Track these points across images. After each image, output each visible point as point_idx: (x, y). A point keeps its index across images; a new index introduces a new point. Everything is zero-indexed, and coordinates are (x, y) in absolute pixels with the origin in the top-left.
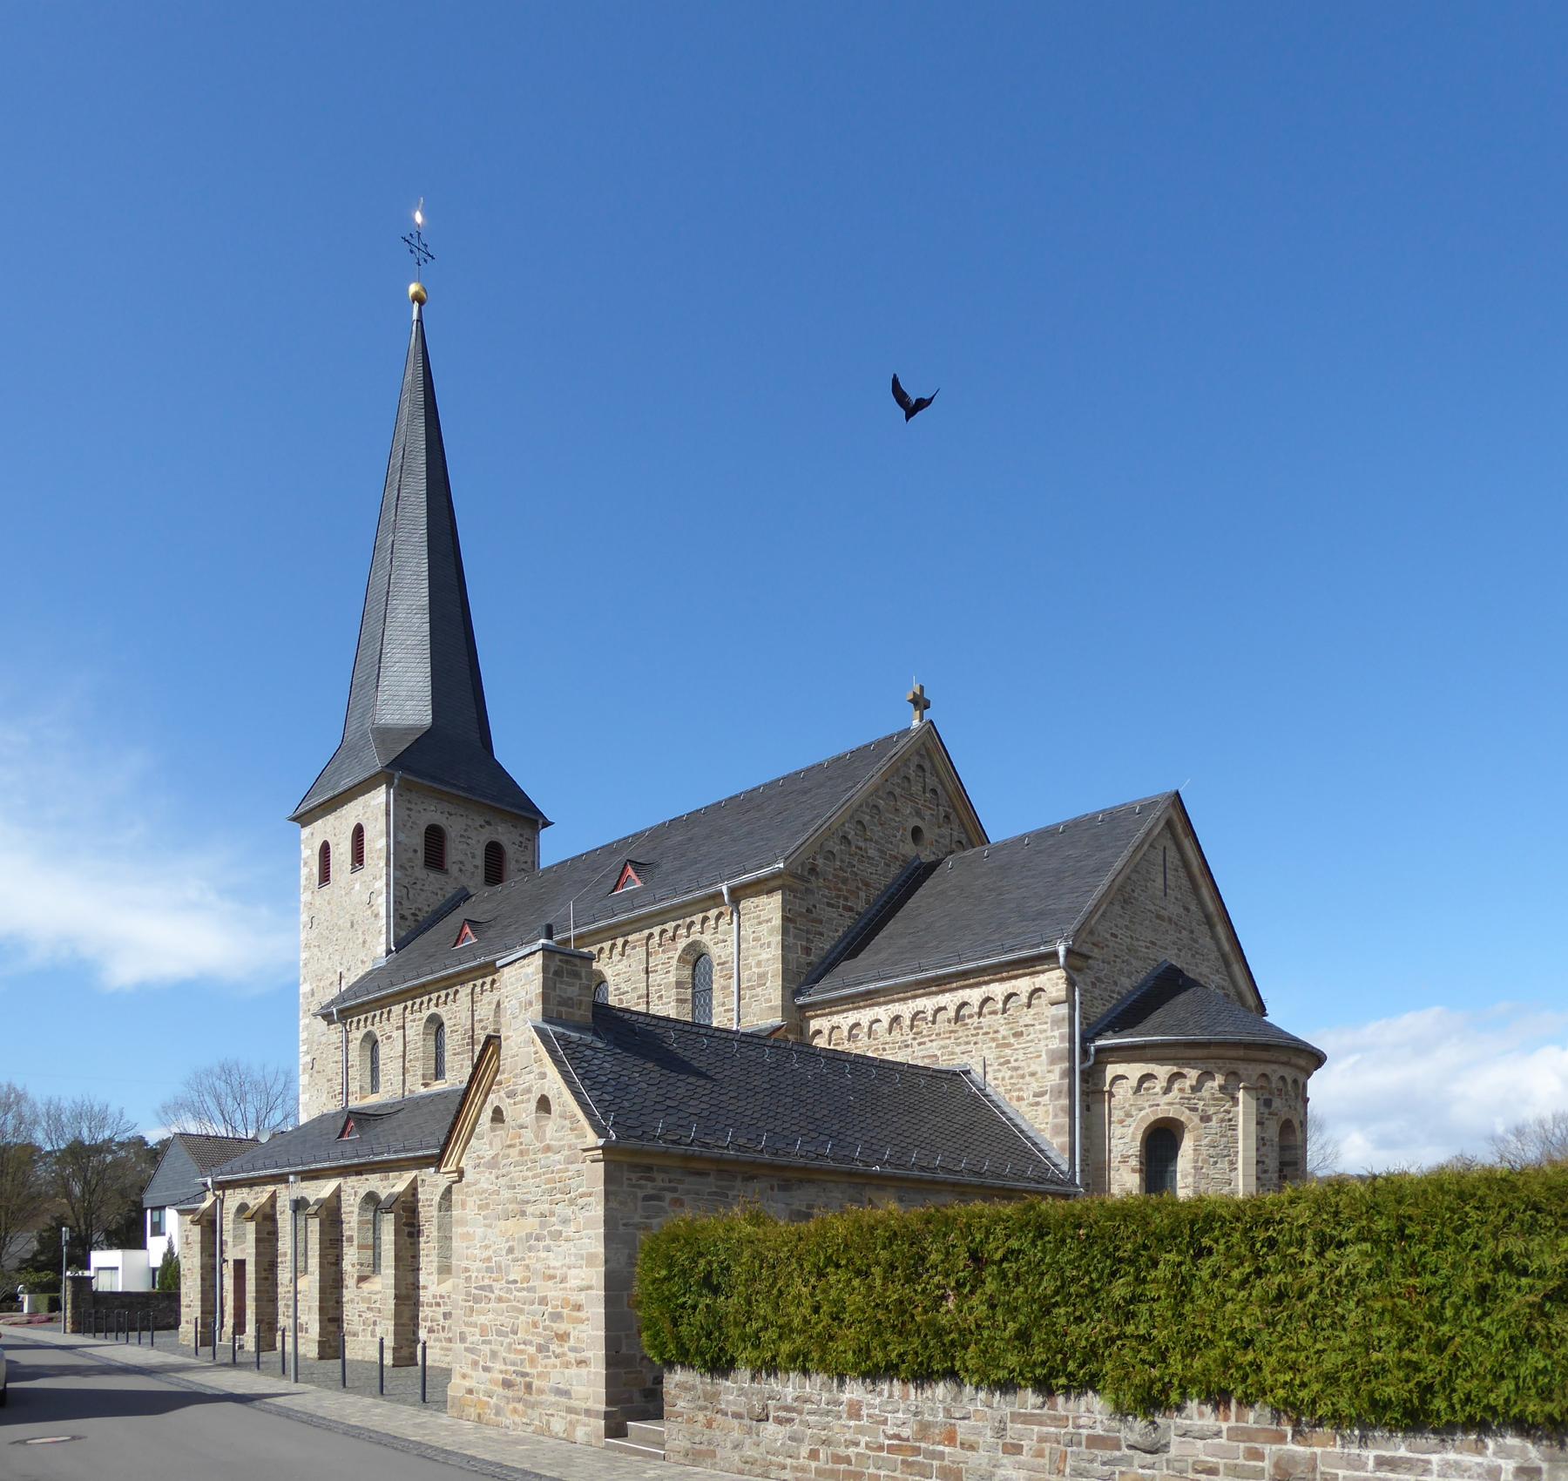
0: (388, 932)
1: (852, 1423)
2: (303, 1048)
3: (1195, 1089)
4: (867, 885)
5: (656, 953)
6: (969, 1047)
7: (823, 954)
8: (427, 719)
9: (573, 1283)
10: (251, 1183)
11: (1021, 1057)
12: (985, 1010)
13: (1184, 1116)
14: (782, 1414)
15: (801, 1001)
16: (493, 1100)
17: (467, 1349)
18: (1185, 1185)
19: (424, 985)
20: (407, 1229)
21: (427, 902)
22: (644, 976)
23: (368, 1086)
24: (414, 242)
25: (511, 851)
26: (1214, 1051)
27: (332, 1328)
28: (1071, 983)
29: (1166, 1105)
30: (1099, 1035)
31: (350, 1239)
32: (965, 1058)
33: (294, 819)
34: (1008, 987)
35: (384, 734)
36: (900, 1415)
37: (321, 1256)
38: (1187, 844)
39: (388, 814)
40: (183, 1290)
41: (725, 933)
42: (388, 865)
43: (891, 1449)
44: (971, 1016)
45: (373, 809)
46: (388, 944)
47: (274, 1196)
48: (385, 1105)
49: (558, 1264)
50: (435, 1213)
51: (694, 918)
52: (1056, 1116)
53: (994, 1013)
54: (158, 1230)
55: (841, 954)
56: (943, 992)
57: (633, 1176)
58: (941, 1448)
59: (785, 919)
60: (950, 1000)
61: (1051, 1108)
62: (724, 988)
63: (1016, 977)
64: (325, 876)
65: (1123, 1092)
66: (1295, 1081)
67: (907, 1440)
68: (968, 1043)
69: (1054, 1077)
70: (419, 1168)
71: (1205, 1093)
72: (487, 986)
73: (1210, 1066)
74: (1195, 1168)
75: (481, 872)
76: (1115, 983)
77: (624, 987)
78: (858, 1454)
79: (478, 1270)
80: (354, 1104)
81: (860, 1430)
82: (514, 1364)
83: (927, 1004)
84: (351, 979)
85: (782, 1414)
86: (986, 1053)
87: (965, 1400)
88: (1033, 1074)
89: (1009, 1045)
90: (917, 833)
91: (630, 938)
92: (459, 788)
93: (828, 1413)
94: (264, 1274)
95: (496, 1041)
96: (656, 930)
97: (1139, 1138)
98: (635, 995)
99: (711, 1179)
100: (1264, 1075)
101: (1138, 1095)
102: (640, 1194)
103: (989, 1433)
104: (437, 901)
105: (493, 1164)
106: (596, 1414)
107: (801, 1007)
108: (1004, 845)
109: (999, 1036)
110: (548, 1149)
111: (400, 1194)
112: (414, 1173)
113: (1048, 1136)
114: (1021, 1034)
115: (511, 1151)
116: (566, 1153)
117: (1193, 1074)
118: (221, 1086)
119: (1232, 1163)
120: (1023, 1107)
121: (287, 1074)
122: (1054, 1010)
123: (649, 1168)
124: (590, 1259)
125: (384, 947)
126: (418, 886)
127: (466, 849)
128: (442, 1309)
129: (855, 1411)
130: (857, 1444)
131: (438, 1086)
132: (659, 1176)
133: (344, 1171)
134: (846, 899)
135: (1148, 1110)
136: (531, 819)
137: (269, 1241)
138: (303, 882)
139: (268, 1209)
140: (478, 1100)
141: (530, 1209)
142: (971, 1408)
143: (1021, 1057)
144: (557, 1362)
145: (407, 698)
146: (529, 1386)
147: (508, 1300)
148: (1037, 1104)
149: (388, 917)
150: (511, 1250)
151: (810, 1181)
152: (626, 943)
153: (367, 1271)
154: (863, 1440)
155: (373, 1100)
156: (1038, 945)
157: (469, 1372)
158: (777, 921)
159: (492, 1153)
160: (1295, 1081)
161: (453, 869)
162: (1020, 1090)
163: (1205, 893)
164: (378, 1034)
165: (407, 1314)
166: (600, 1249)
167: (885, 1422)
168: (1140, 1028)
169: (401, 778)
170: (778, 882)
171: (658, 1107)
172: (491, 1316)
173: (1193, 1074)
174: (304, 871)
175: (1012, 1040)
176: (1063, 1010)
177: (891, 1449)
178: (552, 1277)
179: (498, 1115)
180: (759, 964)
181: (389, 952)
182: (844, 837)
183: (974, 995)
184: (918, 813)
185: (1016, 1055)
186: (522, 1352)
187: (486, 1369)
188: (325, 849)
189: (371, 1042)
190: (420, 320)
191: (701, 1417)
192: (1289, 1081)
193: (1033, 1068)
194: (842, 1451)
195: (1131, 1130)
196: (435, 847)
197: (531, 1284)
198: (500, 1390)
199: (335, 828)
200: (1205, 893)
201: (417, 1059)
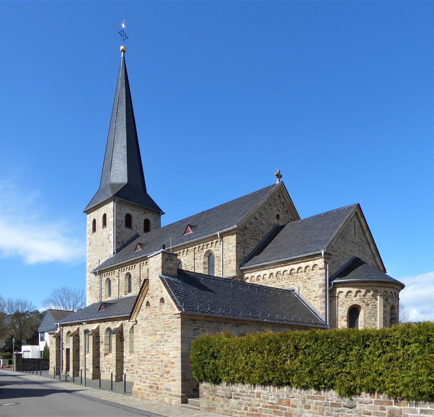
0: (114, 247)
1: (258, 399)
2: (87, 283)
3: (364, 296)
4: (262, 232)
5: (197, 253)
8: (126, 181)
9: (171, 356)
10: (71, 325)
11: (310, 286)
12: (299, 271)
13: (361, 304)
14: (236, 396)
15: (242, 268)
16: (147, 299)
17: (138, 376)
18: (361, 325)
19: (125, 263)
23: (108, 295)
24: (122, 33)
25: (152, 222)
27: (97, 370)
28: (326, 263)
30: (334, 279)
32: (293, 286)
33: (85, 212)
35: (113, 186)
36: (273, 396)
37: (93, 347)
38: (362, 220)
39: (114, 210)
40: (50, 358)
41: (218, 247)
42: (114, 226)
43: (270, 407)
44: (295, 273)
45: (109, 209)
48: (113, 301)
50: (129, 334)
51: (209, 243)
52: (321, 304)
54: (42, 339)
55: (254, 254)
56: (286, 265)
58: (285, 407)
59: (237, 243)
60: (288, 268)
61: (319, 301)
62: (218, 264)
64: (94, 230)
65: (342, 297)
66: (395, 293)
67: (275, 404)
68: (294, 281)
69: (320, 292)
71: (367, 297)
72: (145, 264)
74: (364, 320)
75: (143, 229)
76: (339, 263)
77: (187, 264)
78: (260, 409)
79: (142, 352)
80: (103, 300)
81: (260, 401)
82: (153, 381)
83: (281, 269)
84: (102, 261)
85: (236, 396)
86: (299, 284)
87: (293, 392)
88: (314, 291)
89: (306, 282)
90: (278, 216)
91: (189, 249)
92: (136, 202)
94: (75, 353)
96: (197, 246)
97: (347, 311)
98: (190, 266)
99: (214, 323)
102: (192, 328)
103: (300, 402)
104: (129, 238)
105: (146, 319)
106: (178, 396)
108: (305, 220)
110: (163, 314)
111: (117, 328)
112: (122, 322)
113: (318, 310)
114: (310, 279)
115: (152, 315)
116: (169, 315)
117: (363, 291)
118: (62, 295)
119: (376, 318)
120: (311, 301)
121: (83, 291)
122: (320, 271)
123: (195, 320)
124: (177, 348)
126: (123, 233)
128: (131, 364)
129: (259, 395)
130: (259, 406)
131: (129, 295)
133: (100, 321)
134: (256, 237)
136: (158, 212)
137: (77, 342)
138: (87, 231)
139: (77, 333)
140: (142, 299)
141: (158, 333)
142: (295, 395)
143: (310, 286)
144: (166, 380)
145: (120, 175)
146: (157, 388)
147: (151, 361)
148: (315, 300)
149: (114, 242)
150: (152, 346)
153: (107, 352)
154: (261, 404)
155: (109, 299)
156: (315, 251)
157: (139, 383)
159: (146, 315)
160: (395, 293)
161: (134, 228)
162: (310, 296)
164: (111, 279)
165: (120, 365)
167: (268, 399)
168: (347, 277)
171: (197, 301)
172: (146, 366)
173: (363, 291)
174: (88, 228)
175: (307, 280)
176: (323, 271)
177: (270, 407)
178: (165, 354)
179: (148, 304)
180: (229, 257)
181: (114, 253)
182: (255, 218)
183: (296, 267)
184: (278, 210)
185: (308, 285)
186: (155, 377)
187: (144, 382)
188: (94, 221)
190: (124, 57)
191: (211, 397)
192: (393, 293)
193: (314, 289)
194: (255, 408)
195: (344, 308)
197: (158, 356)
198: (148, 389)
199: (98, 215)
201: (123, 286)
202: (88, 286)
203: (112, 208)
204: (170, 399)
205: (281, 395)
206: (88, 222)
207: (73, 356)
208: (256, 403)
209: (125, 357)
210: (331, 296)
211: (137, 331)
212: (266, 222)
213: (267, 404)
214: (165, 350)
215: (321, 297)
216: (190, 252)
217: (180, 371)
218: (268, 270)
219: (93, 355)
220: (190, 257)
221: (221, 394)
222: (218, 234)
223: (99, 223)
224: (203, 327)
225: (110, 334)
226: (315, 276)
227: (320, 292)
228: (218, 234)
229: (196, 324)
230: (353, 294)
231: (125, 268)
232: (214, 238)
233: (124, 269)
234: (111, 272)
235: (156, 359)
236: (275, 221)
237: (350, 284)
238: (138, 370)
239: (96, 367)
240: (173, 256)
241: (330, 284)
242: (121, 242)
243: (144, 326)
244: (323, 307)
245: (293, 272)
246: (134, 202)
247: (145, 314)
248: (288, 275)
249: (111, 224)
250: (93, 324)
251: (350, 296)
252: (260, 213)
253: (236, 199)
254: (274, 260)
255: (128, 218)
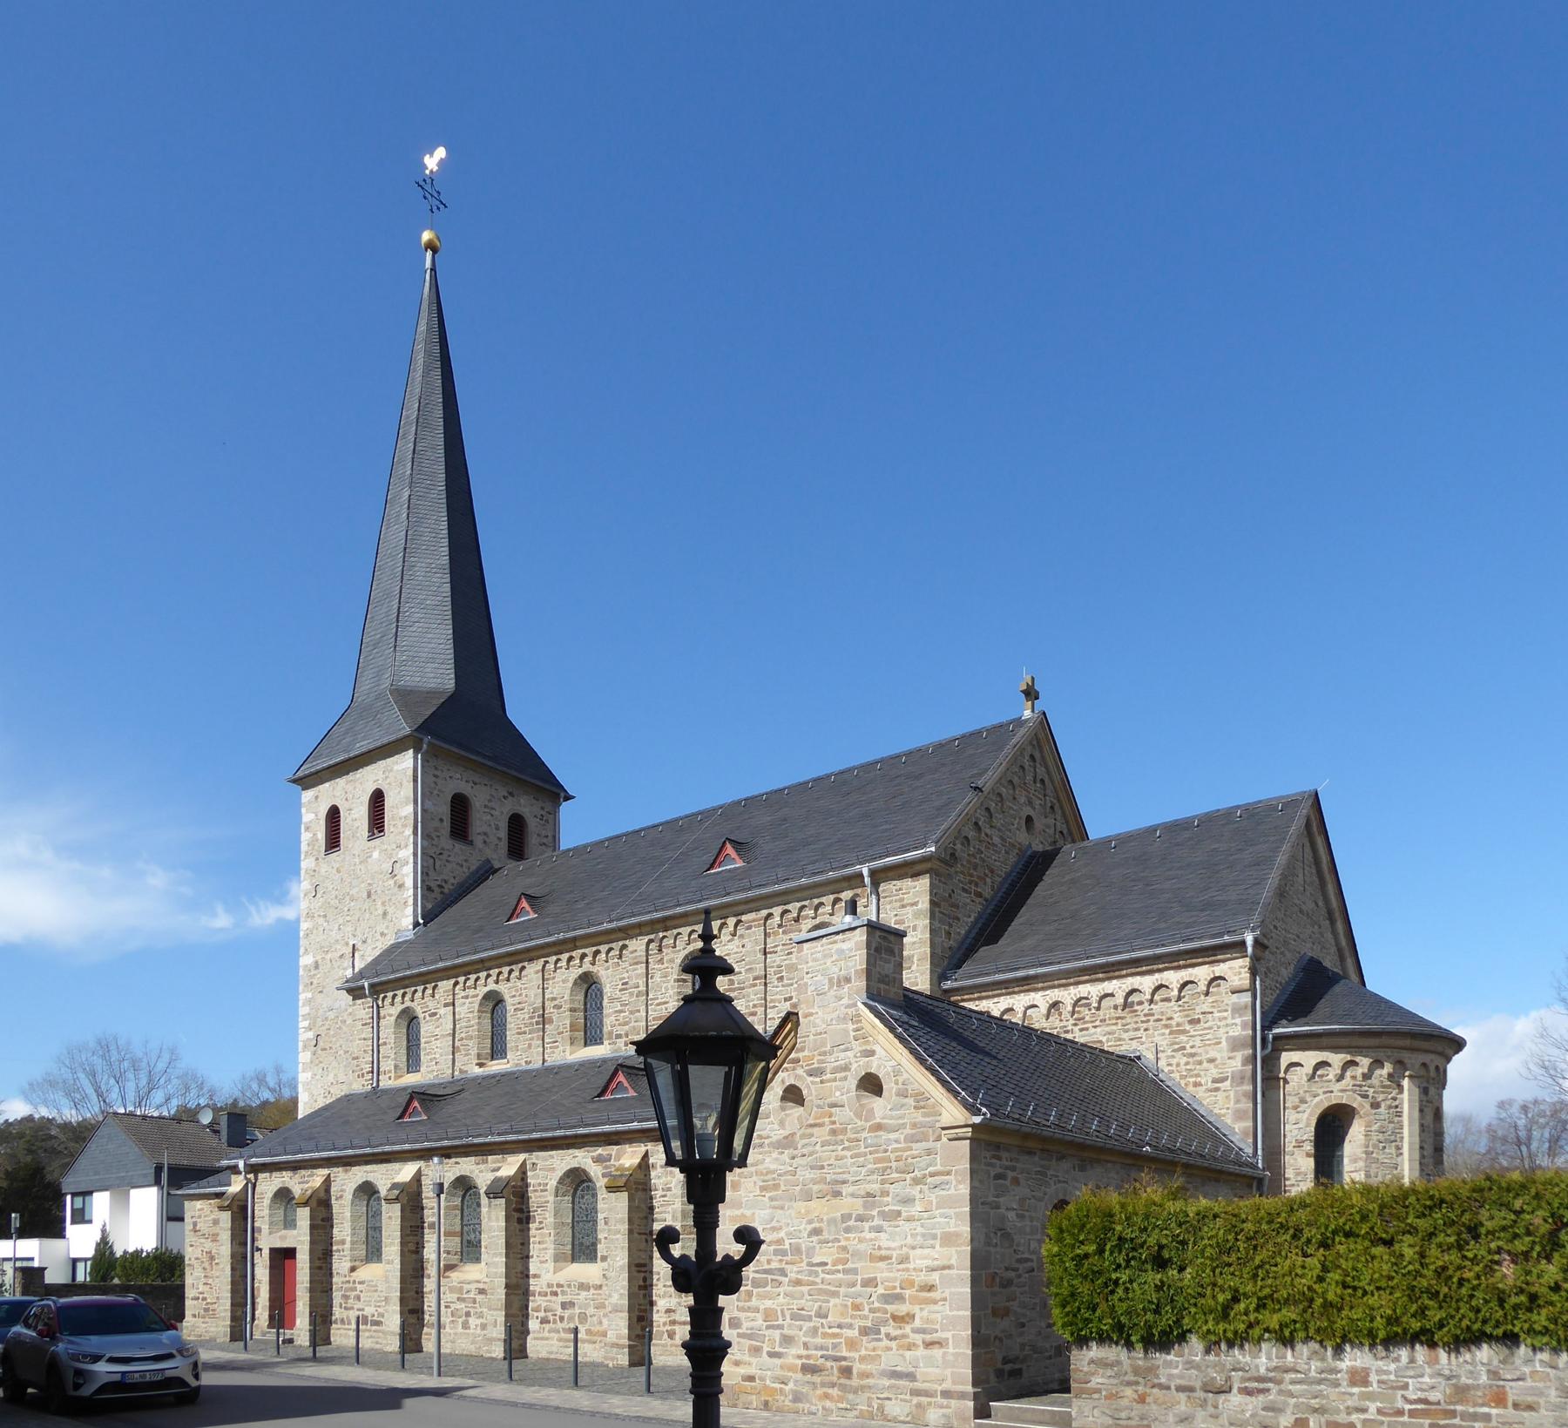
0: (415, 904)
1: (1355, 1390)
2: (303, 1024)
3: (1366, 1077)
4: (992, 871)
5: (776, 934)
6: (1138, 1034)
7: (959, 938)
8: (450, 684)
10: (295, 1167)
11: (1198, 1043)
12: (1156, 997)
13: (1356, 1102)
15: (948, 985)
18: (1354, 1164)
19: (482, 961)
20: (516, 1215)
21: (453, 874)
22: (760, 956)
23: (403, 1065)
24: (426, 185)
25: (532, 824)
26: (1385, 1040)
27: (412, 1320)
28: (1253, 972)
29: (1338, 1092)
31: (434, 1227)
32: (1134, 1044)
33: (294, 781)
34: (1185, 975)
35: (405, 697)
36: (1426, 1379)
37: (402, 1244)
38: (1320, 841)
39: (415, 781)
40: (189, 1280)
43: (1412, 1413)
44: (1140, 1003)
45: (398, 775)
46: (415, 916)
47: (327, 1182)
48: (434, 1085)
49: (893, 1245)
50: (551, 1198)
51: (823, 899)
52: (1238, 1101)
53: (1168, 1000)
54: (81, 1217)
55: (976, 940)
56: (1110, 979)
57: (988, 1154)
58: (1485, 1410)
59: (932, 902)
60: (1119, 987)
61: (1232, 1094)
63: (1193, 966)
64: (333, 840)
66: (1437, 1068)
67: (1438, 1403)
68: (1137, 1029)
70: (529, 1150)
71: (1375, 1081)
72: (563, 964)
73: (1381, 1055)
74: (1366, 1153)
75: (504, 845)
78: (1365, 1421)
80: (386, 1083)
81: (1371, 1397)
82: (822, 1348)
83: (1092, 990)
86: (1157, 1039)
87: (1518, 1362)
88: (1212, 1061)
89: (1184, 1032)
91: (744, 918)
92: (485, 756)
93: (1320, 1382)
94: (318, 1263)
95: (794, 1018)
96: (777, 911)
99: (1036, 1159)
100: (1424, 1065)
101: (1313, 1080)
103: (1553, 1393)
104: (462, 874)
107: (946, 991)
108: (1105, 842)
109: (1173, 1023)
110: (879, 1127)
111: (510, 1179)
112: (522, 1157)
113: (1229, 1121)
114: (1199, 1021)
116: (908, 1131)
117: (1365, 1062)
118: (98, 1062)
119: (1398, 1148)
120: (1200, 1093)
121: (172, 1051)
123: (998, 1147)
124: (948, 1239)
125: (411, 919)
126: (444, 857)
127: (489, 821)
128: (560, 1298)
129: (1359, 1378)
130: (1364, 1410)
131: (496, 1067)
132: (1005, 1155)
133: (425, 1155)
135: (1322, 1097)
136: (552, 792)
137: (324, 1227)
138: (304, 847)
139: (322, 1194)
141: (846, 1189)
142: (1527, 1370)
143: (1198, 1043)
146: (847, 1372)
147: (814, 1283)
148: (1217, 1089)
149: (415, 887)
151: (1098, 1161)
152: (739, 922)
156: (1221, 935)
158: (924, 903)
160: (1437, 1068)
161: (478, 841)
162: (1198, 1075)
163: (1331, 888)
164: (419, 1011)
165: (516, 1305)
166: (965, 1229)
167: (1405, 1387)
168: (1312, 1016)
169: (429, 744)
170: (929, 865)
173: (1365, 1062)
174: (305, 837)
175: (1188, 1027)
176: (1246, 998)
178: (882, 1259)
179: (793, 1095)
181: (416, 924)
182: (976, 824)
183: (1146, 983)
184: (1030, 803)
185: (1192, 1041)
186: (835, 1335)
188: (334, 816)
189: (409, 1020)
190: (433, 269)
191: (1129, 1392)
192: (1432, 1068)
193: (1212, 1054)
195: (1306, 1115)
196: (460, 816)
197: (850, 1265)
198: (799, 1376)
199: (350, 794)
200: (1331, 888)
201: (471, 1038)
202: (305, 1036)
203: (410, 772)
204: (919, 1405)
205: (1462, 1372)
206: (307, 817)
207: (311, 1275)
208: (1349, 1403)
209: (535, 1276)
210: (1268, 1078)
211: (736, 1186)
212: (1002, 839)
213: (1400, 1404)
214: (884, 1244)
215: (1238, 1079)
216: (749, 928)
217: (968, 1313)
218: (1041, 993)
219: (402, 1270)
220: (749, 947)
221: (1179, 1382)
222: (865, 872)
223: (355, 818)
224: (1013, 1169)
225: (464, 1197)
226: (1217, 1015)
227: (1233, 1063)
228: (865, 872)
229: (999, 1158)
230: (1332, 1073)
231: (483, 975)
232: (845, 884)
233: (477, 979)
234: (420, 988)
235: (840, 1275)
236: (1022, 837)
237: (1325, 1041)
238: (742, 1315)
239: (412, 1312)
240: (892, 938)
241: (1264, 1040)
242: (437, 890)
243: (773, 1167)
244: (1245, 1112)
245: (1134, 998)
246: (478, 753)
247: (776, 1126)
248: (1116, 1007)
249: (405, 826)
250: (396, 1166)
251: (1321, 1076)
252: (988, 809)
253: (878, 757)
254: (1068, 961)
255: (460, 806)
